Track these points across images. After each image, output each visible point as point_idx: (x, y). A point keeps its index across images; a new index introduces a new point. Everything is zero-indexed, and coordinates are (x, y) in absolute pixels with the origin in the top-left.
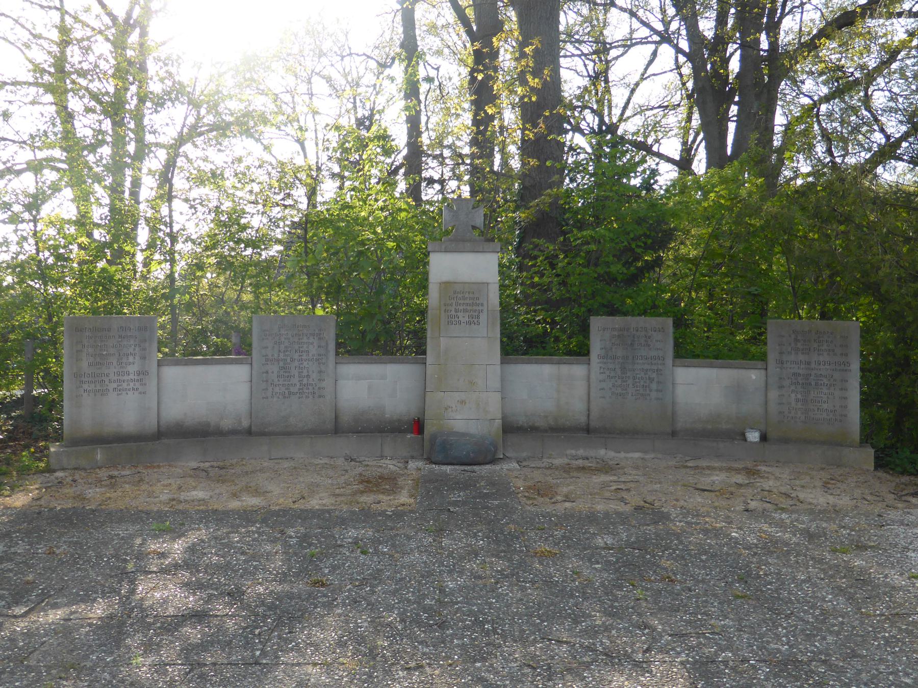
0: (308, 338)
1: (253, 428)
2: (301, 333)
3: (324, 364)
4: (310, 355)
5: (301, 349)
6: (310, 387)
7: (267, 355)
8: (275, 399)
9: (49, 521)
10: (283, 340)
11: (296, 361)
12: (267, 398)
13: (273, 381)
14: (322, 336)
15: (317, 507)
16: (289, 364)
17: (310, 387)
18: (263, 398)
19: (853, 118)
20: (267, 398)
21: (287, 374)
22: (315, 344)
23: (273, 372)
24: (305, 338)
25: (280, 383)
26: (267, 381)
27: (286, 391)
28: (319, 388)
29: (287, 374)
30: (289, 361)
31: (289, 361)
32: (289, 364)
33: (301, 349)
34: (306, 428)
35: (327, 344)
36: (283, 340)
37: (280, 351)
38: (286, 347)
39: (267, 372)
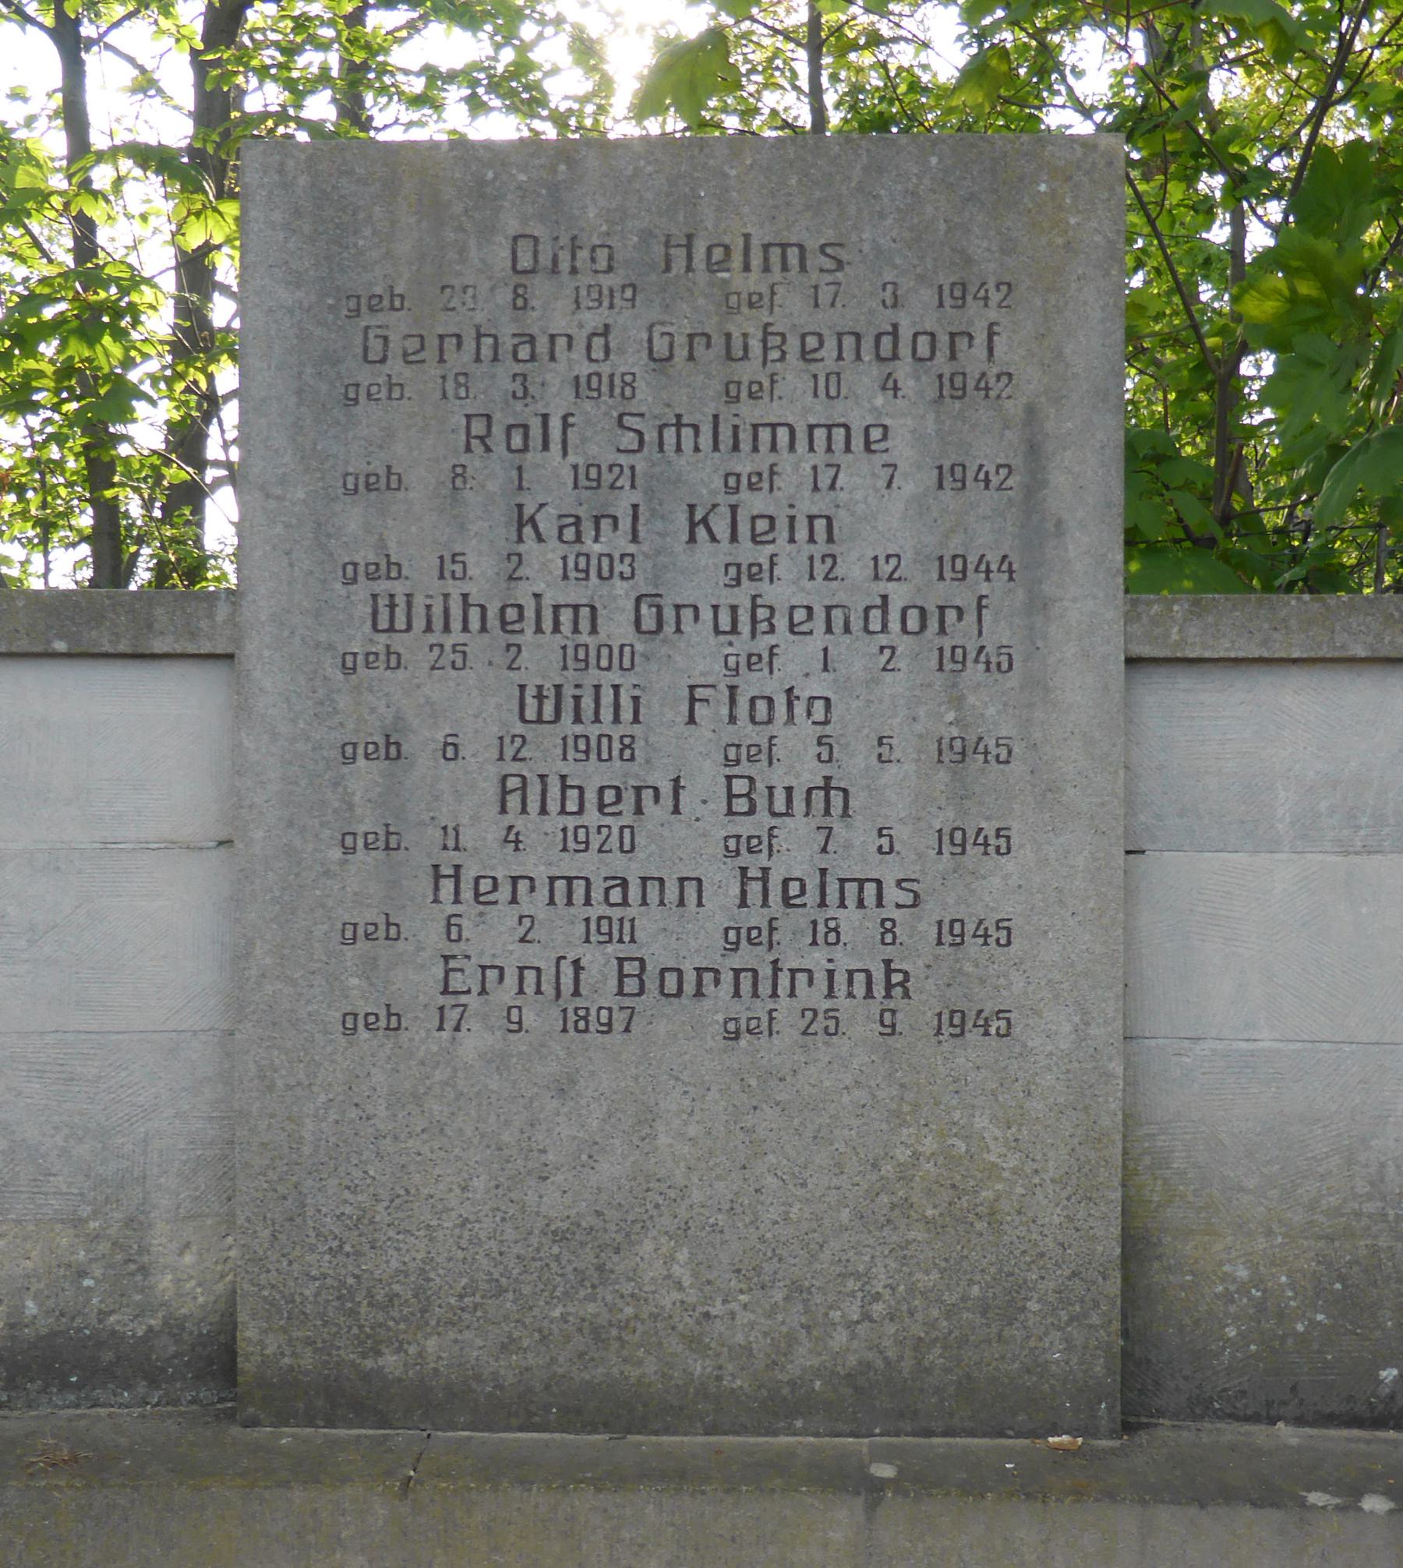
0: (830, 388)
1: (249, 1332)
2: (747, 324)
3: (999, 665)
4: (854, 567)
5: (754, 503)
6: (849, 919)
7: (392, 569)
8: (475, 1041)
9: (775, 354)
10: (558, 401)
11: (698, 633)
12: (393, 1022)
13: (451, 835)
14: (973, 359)
15: (1160, 1308)
16: (623, 659)
17: (849, 919)
18: (350, 1024)
19: (729, 101)
20: (393, 1022)
21: (594, 775)
22: (901, 448)
23: (451, 750)
24: (794, 379)
25: (536, 863)
26: (389, 842)
27: (599, 961)
28: (951, 933)
29: (594, 775)
30: (617, 628)
31: (617, 628)
32: (623, 659)
33: (754, 503)
34: (803, 1358)
35: (1034, 450)
36: (558, 401)
37: (523, 521)
38: (589, 478)
39: (391, 749)
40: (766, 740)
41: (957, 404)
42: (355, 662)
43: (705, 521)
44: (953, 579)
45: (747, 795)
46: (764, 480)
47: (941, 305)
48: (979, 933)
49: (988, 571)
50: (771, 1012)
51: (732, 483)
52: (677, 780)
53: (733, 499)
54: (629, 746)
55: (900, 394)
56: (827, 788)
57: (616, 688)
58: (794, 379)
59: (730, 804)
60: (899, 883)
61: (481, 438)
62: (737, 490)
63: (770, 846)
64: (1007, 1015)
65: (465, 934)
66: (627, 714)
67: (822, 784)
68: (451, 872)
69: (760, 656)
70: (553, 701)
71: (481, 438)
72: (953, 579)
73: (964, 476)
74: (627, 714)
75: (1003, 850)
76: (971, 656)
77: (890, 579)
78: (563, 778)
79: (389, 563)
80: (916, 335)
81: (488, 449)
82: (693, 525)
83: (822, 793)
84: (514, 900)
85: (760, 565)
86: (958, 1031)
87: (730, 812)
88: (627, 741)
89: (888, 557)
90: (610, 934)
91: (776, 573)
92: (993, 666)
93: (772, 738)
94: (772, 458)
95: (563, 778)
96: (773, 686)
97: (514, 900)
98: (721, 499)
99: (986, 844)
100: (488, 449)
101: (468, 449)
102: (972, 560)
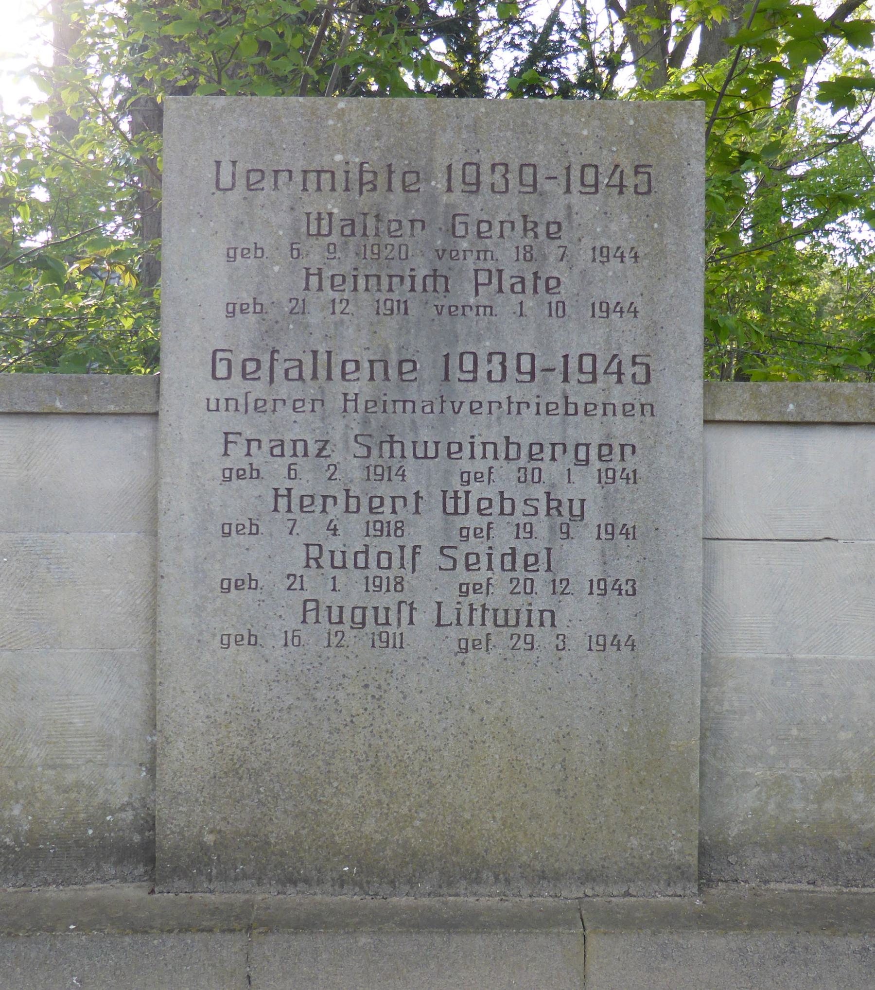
40: (487, 470)
44: (598, 595)
49: (619, 645)
50: (489, 579)
53: (467, 488)
54: (400, 583)
60: (536, 513)
61: (316, 560)
62: (468, 482)
63: (488, 534)
68: (285, 492)
69: (482, 530)
71: (316, 560)
72: (598, 595)
76: (609, 642)
77: (562, 593)
79: (252, 470)
80: (581, 356)
81: (319, 566)
83: (510, 558)
84: (324, 510)
85: (481, 585)
86: (610, 537)
88: (399, 525)
89: (561, 580)
90: (387, 642)
91: (492, 477)
92: (623, 592)
93: (488, 634)
94: (489, 574)
96: (491, 492)
97: (324, 510)
99: (620, 590)
100: (319, 566)
101: (308, 566)
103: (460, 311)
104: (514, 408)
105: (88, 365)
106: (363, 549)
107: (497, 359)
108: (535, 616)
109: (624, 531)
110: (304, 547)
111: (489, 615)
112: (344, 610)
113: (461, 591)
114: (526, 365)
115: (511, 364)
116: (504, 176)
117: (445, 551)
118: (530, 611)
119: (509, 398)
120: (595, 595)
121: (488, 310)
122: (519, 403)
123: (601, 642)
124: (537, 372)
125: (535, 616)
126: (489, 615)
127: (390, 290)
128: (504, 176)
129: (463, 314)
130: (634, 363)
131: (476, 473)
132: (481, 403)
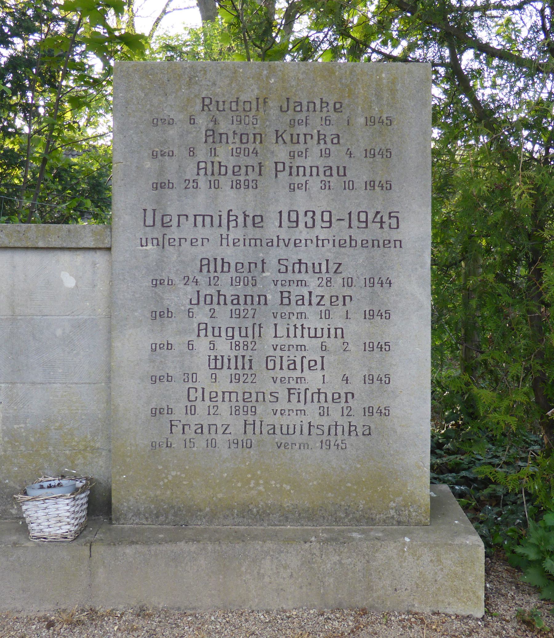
41: (372, 159)
42: (156, 411)
43: (281, 136)
45: (288, 297)
46: (304, 154)
47: (365, 415)
48: (379, 282)
49: (382, 283)
51: (292, 156)
52: (263, 261)
55: (352, 156)
56: (319, 393)
57: (243, 357)
58: (315, 150)
59: (282, 301)
64: (389, 312)
65: (175, 186)
66: (247, 366)
67: (317, 391)
70: (221, 361)
73: (373, 378)
74: (247, 366)
75: (387, 414)
78: (220, 163)
82: (277, 138)
83: (317, 395)
87: (282, 303)
91: (307, 186)
95: (220, 163)
98: (288, 129)
99: (382, 315)
102: (377, 150)
103: (287, 316)
104: (320, 243)
105: (6, 30)
106: (235, 100)
107: (310, 214)
108: (332, 331)
109: (380, 314)
110: (177, 217)
111: (306, 332)
112: (210, 225)
113: (290, 156)
114: (326, 217)
115: (318, 217)
116: (312, 217)
117: (273, 394)
118: (329, 329)
119: (317, 237)
120: (367, 351)
121: (303, 347)
122: (323, 240)
123: (371, 346)
124: (333, 220)
125: (332, 331)
126: (306, 332)
127: (247, 174)
128: (312, 217)
129: (289, 318)
130: (385, 345)
131: (301, 110)
132: (301, 240)
